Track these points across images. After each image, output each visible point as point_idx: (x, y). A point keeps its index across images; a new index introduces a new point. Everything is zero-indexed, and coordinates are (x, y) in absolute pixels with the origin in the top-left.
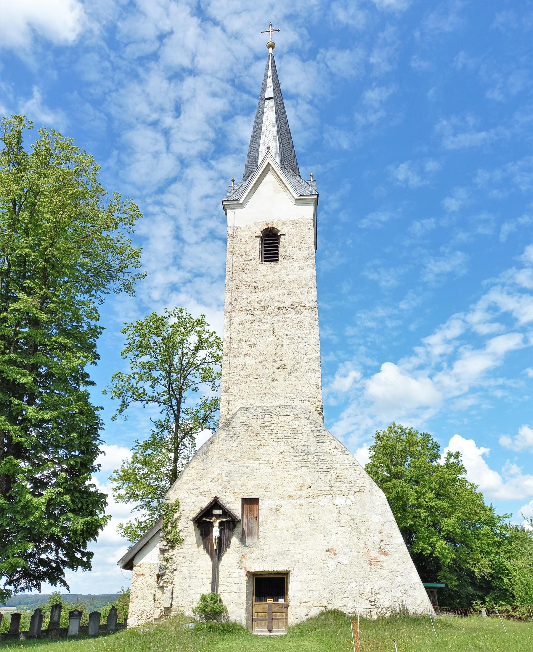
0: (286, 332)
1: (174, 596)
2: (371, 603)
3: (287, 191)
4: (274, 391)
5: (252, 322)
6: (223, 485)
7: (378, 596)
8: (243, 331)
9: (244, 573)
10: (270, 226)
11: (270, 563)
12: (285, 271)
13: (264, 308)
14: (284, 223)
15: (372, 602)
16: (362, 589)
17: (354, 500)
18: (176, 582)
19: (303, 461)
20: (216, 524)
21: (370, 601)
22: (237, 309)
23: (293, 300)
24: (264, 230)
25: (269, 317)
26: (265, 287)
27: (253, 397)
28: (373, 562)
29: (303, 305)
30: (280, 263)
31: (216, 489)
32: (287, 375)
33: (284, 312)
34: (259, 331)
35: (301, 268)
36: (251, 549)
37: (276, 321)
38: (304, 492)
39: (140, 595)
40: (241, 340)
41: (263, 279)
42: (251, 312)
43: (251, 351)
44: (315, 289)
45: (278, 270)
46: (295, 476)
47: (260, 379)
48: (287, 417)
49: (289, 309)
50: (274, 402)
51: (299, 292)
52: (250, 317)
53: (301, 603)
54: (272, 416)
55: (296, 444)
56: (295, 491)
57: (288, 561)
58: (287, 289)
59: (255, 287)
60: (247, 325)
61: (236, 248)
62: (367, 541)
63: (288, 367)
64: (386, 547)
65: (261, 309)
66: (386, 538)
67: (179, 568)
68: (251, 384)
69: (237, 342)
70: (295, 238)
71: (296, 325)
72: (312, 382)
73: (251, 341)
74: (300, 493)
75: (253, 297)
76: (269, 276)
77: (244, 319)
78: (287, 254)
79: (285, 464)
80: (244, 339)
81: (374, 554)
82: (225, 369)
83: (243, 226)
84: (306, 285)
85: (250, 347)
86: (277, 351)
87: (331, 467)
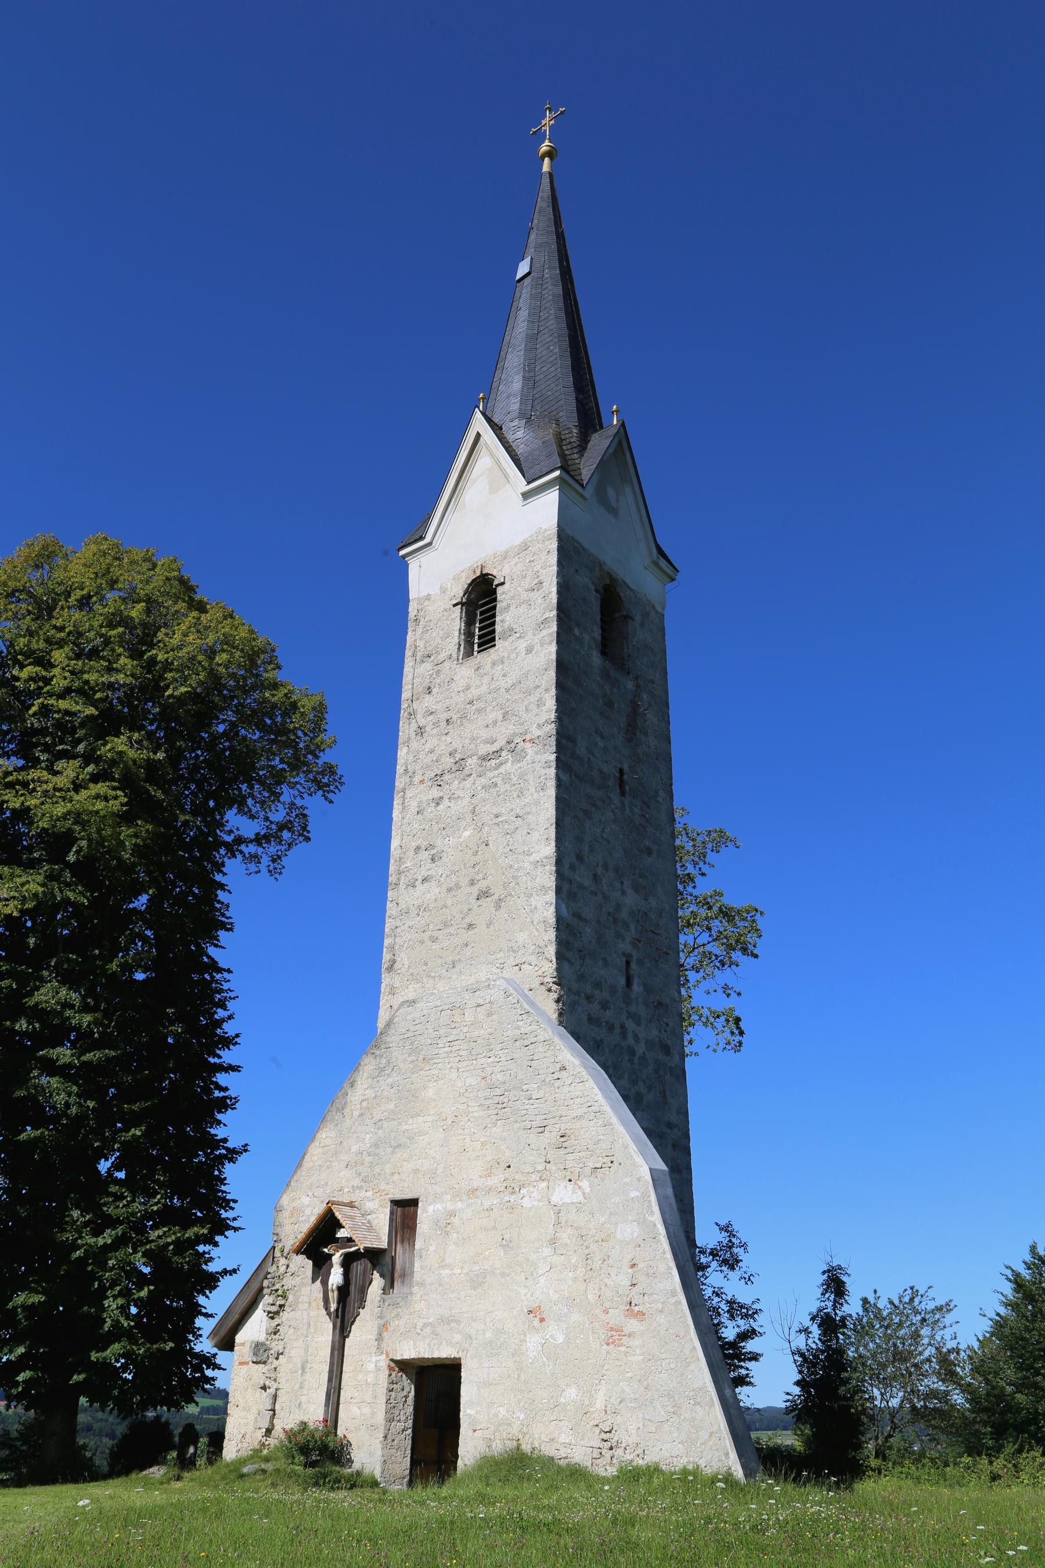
0: (495, 811)
1: (277, 1407)
4: (468, 952)
5: (438, 802)
7: (619, 1419)
9: (383, 1362)
11: (427, 1341)
14: (505, 556)
16: (587, 1402)
17: (588, 1190)
19: (500, 1106)
22: (417, 779)
24: (470, 585)
27: (433, 974)
28: (615, 1336)
29: (528, 737)
31: (352, 1183)
32: (493, 910)
33: (493, 762)
37: (479, 788)
39: (241, 1405)
42: (438, 780)
45: (488, 667)
46: (483, 1144)
48: (479, 1009)
52: (435, 793)
53: (475, 1431)
54: (453, 1012)
55: (489, 1070)
56: (481, 1177)
57: (458, 1338)
60: (430, 811)
61: (421, 644)
62: (603, 1287)
64: (640, 1301)
67: (287, 1350)
70: (522, 584)
71: (513, 788)
72: (537, 917)
79: (467, 1119)
82: (391, 920)
83: (434, 591)
86: (477, 858)
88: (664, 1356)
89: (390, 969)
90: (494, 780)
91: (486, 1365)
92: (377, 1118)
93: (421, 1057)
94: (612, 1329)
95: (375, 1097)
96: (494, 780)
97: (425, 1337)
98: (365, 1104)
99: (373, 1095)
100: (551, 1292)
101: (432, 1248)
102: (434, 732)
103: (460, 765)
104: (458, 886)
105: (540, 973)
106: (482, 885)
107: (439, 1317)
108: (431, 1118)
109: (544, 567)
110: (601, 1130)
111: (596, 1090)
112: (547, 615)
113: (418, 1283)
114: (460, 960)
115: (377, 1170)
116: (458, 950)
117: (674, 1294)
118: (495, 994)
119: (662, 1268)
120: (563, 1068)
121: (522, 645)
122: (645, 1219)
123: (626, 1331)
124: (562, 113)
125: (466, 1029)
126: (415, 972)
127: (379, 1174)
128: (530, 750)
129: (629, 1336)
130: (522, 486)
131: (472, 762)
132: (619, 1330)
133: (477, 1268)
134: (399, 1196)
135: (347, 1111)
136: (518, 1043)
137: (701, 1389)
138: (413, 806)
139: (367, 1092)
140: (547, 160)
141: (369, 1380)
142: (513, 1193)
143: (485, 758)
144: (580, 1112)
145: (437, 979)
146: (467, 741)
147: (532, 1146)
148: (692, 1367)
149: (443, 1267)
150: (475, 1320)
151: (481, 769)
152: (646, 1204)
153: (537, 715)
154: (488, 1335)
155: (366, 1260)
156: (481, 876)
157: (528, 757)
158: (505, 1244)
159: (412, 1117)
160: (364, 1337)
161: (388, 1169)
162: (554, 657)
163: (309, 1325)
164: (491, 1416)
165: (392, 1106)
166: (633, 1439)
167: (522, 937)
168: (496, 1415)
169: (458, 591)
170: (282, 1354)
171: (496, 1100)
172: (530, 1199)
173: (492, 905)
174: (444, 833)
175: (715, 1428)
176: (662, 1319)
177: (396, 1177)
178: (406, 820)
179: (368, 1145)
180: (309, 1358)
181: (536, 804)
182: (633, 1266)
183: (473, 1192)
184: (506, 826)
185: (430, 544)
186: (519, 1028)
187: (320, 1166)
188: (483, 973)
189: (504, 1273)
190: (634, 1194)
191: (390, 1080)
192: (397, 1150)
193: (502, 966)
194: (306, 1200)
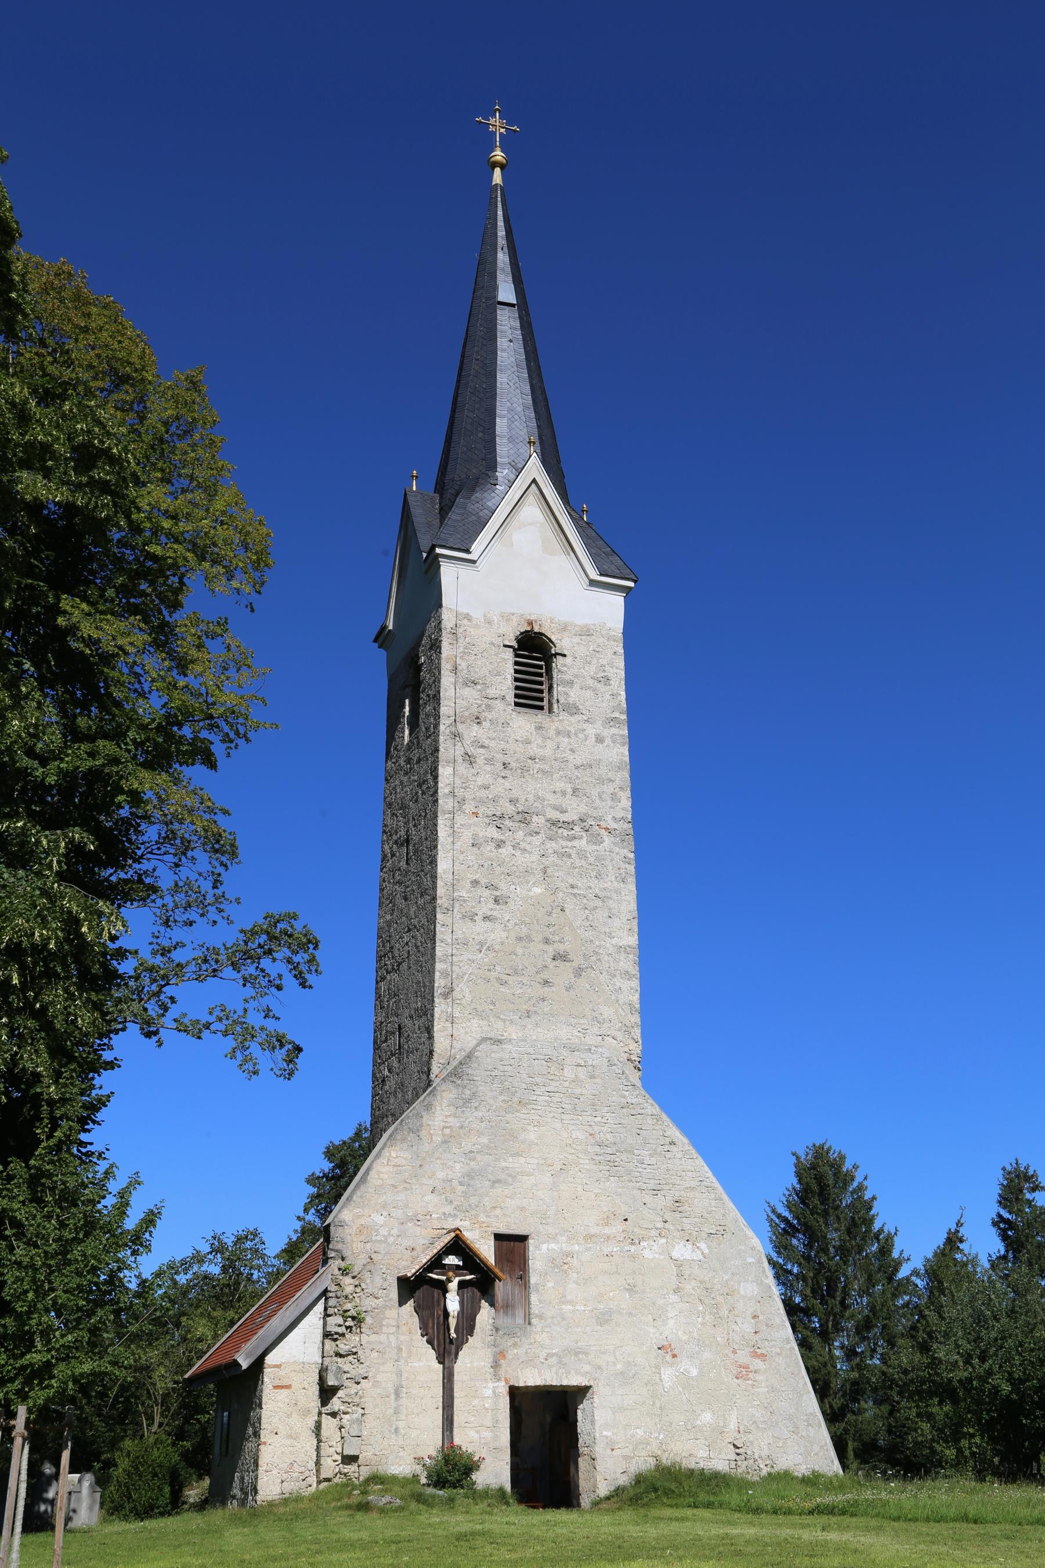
0: (571, 881)
2: (738, 1451)
3: (572, 554)
4: (546, 1007)
5: (500, 844)
6: (455, 1203)
7: (751, 1437)
8: (481, 862)
9: (504, 1391)
10: (536, 629)
12: (566, 740)
13: (524, 817)
14: (564, 628)
15: (738, 1448)
17: (706, 1251)
18: (368, 1402)
19: (612, 1164)
20: (453, 1286)
21: (734, 1445)
22: (469, 808)
23: (583, 809)
24: (522, 633)
25: (537, 840)
26: (525, 770)
27: (502, 1016)
28: (743, 1372)
30: (556, 719)
31: (442, 1210)
32: (572, 976)
33: (566, 833)
34: (514, 868)
35: (600, 740)
36: (516, 1339)
37: (550, 851)
38: (616, 1228)
39: (283, 1430)
40: (475, 883)
41: (520, 748)
42: (497, 820)
43: (497, 911)
44: (628, 793)
45: (552, 732)
47: (515, 978)
48: (580, 1068)
49: (575, 828)
50: (546, 1032)
51: (594, 793)
52: (493, 832)
53: (613, 1450)
54: (550, 1064)
56: (598, 1225)
58: (570, 780)
59: (504, 764)
60: (489, 848)
61: (463, 665)
63: (575, 959)
65: (517, 817)
66: (764, 1328)
68: (497, 985)
69: (468, 885)
71: (590, 867)
72: (623, 998)
73: (496, 889)
74: (607, 1231)
75: (500, 787)
76: (534, 746)
77: (481, 834)
78: (571, 700)
79: (577, 1169)
80: (484, 881)
81: (743, 1356)
82: (443, 945)
83: (477, 615)
84: (611, 780)
85: (496, 901)
86: (552, 920)
87: (663, 1182)
88: (783, 1389)
89: (448, 993)
90: (567, 850)
91: (620, 1393)
92: (468, 1148)
93: (516, 1100)
94: (740, 1366)
95: (461, 1127)
96: (567, 850)
97: (550, 1367)
98: (447, 1131)
99: (458, 1125)
100: (679, 1333)
101: (550, 1285)
102: (488, 768)
103: (524, 817)
104: (529, 938)
105: (626, 1049)
106: (561, 948)
107: (564, 1348)
108: (536, 1161)
109: (611, 664)
110: (714, 1203)
111: (706, 1168)
112: (617, 715)
113: (537, 1316)
114: (536, 1012)
115: (473, 1200)
116: (533, 1001)
117: (788, 1341)
118: (593, 1059)
119: (778, 1321)
120: (672, 1143)
121: (591, 730)
122: (762, 1281)
123: (752, 1368)
124: (515, 131)
125: (566, 1084)
126: (480, 1008)
127: (477, 1206)
128: (608, 840)
129: (756, 1372)
130: (594, 575)
131: (538, 821)
132: (746, 1367)
133: (602, 1307)
134: (503, 1230)
135: (424, 1133)
136: (624, 1110)
137: (811, 1414)
138: (467, 836)
139: (449, 1120)
140: (497, 171)
141: (487, 1405)
142: (632, 1244)
143: (554, 823)
144: (693, 1184)
145: (507, 1023)
146: (531, 797)
147: (648, 1205)
148: (805, 1397)
149: (563, 1303)
150: (604, 1353)
151: (551, 832)
152: (761, 1269)
153: (611, 807)
154: (619, 1367)
155: (476, 1291)
156: (557, 938)
157: (605, 844)
158: (631, 1289)
159: (511, 1156)
160: (475, 1364)
161: (487, 1201)
162: (627, 759)
163: (400, 1350)
164: (628, 1436)
165: (484, 1140)
166: (765, 1452)
167: (607, 1012)
168: (633, 1436)
169: (510, 635)
170: (366, 1378)
171: (609, 1157)
172: (650, 1251)
173: (571, 970)
174: (509, 878)
175: (823, 1443)
176: (780, 1360)
177: (498, 1211)
178: (458, 845)
179: (459, 1175)
180: (404, 1383)
181: (616, 891)
182: (754, 1317)
183: (589, 1237)
184: (585, 901)
185: (474, 562)
186: (624, 1097)
187: (392, 1185)
188: (564, 1033)
189: (631, 1313)
190: (750, 1260)
191: (479, 1114)
192: (497, 1185)
193: (584, 1031)
194: (380, 1220)
